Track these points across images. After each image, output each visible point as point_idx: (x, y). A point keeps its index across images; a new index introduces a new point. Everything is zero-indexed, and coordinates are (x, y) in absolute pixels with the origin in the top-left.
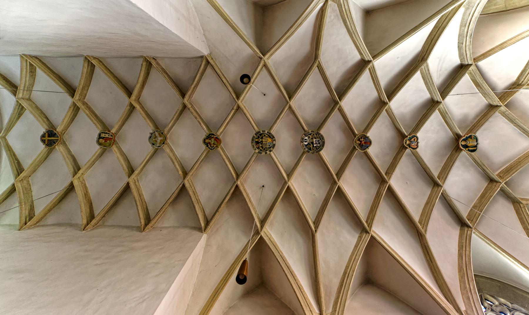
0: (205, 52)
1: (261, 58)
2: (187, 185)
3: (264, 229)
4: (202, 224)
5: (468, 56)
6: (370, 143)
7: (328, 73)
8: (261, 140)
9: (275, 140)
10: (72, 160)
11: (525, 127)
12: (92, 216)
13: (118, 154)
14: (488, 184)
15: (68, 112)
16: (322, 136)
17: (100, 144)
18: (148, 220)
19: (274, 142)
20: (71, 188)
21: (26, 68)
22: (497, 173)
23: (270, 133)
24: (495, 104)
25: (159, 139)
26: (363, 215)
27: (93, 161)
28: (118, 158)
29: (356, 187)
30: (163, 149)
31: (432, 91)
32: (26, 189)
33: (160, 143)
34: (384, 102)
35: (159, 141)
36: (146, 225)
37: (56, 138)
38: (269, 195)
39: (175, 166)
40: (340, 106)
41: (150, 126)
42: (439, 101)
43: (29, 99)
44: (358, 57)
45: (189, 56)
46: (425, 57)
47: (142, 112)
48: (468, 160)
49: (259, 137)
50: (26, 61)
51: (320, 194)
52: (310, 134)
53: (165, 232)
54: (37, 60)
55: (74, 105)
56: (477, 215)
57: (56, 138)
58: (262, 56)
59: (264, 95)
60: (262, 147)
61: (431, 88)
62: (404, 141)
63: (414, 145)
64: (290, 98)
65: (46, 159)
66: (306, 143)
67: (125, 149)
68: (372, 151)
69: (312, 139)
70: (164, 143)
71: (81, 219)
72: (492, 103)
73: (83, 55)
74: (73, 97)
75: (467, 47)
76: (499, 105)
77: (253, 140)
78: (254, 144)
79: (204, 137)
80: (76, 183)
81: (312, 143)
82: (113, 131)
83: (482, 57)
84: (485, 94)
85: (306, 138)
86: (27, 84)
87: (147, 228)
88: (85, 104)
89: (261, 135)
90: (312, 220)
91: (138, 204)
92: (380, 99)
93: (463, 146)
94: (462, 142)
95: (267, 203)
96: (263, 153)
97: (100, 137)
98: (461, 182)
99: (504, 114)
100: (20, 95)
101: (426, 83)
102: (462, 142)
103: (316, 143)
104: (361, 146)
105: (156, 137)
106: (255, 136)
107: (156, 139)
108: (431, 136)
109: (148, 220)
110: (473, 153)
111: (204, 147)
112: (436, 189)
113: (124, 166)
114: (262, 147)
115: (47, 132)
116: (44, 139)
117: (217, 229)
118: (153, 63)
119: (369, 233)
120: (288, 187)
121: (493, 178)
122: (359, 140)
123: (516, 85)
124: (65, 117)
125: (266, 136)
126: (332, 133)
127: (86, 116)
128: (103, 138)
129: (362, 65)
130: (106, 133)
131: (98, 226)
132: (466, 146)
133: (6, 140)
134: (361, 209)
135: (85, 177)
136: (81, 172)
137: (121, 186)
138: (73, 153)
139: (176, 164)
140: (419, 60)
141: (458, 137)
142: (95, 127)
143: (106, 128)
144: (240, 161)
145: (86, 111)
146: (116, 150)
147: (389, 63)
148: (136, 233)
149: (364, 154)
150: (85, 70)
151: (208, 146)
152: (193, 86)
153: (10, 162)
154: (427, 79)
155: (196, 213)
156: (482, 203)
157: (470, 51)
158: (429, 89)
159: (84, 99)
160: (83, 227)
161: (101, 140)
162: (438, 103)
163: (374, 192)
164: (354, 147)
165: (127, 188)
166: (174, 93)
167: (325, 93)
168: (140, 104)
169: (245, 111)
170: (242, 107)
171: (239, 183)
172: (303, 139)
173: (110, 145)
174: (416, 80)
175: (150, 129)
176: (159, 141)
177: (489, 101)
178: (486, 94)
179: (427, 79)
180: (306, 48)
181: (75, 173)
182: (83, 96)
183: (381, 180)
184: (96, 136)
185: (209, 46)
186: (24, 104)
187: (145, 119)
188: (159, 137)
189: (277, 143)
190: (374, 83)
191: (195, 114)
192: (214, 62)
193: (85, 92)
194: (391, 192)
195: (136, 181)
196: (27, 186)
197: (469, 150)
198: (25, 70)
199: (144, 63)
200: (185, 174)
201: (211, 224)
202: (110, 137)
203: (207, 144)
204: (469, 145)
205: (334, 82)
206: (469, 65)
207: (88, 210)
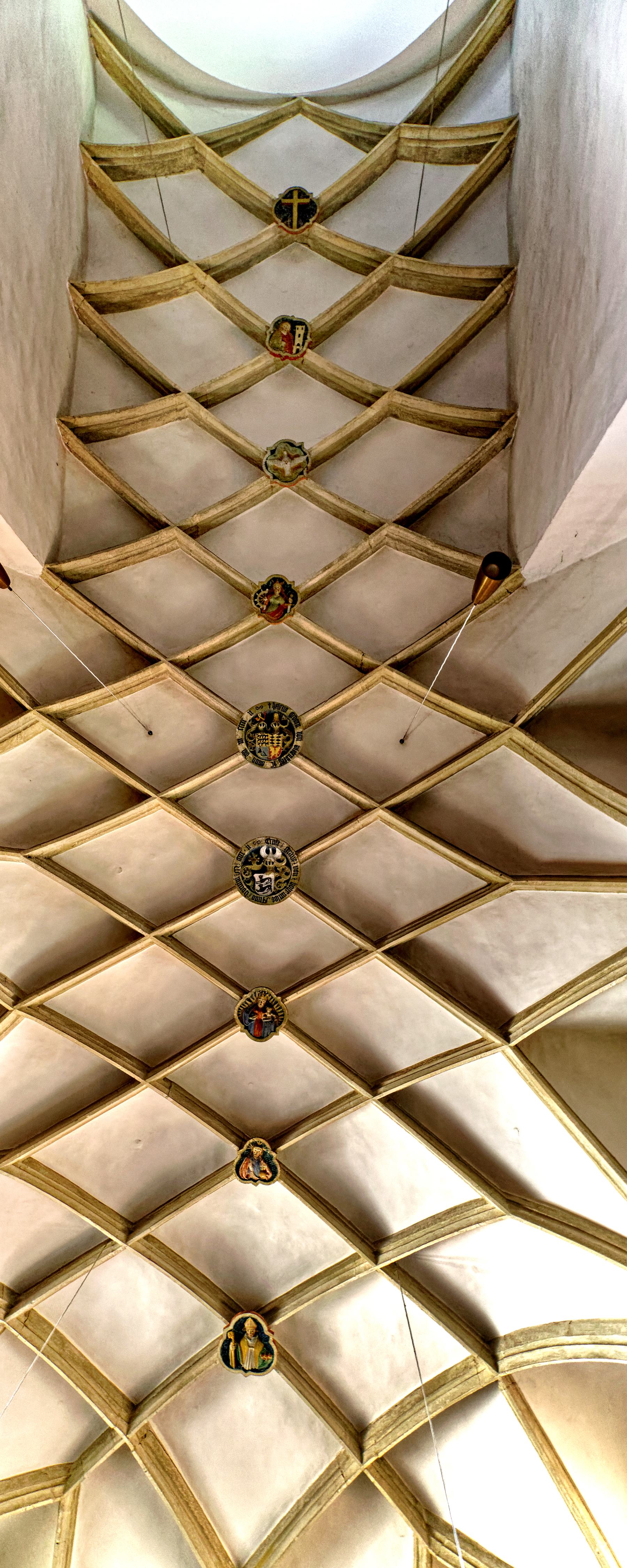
0: (533, 566)
1: (513, 721)
2: (164, 535)
3: (45, 721)
4: (70, 562)
5: (527, 1356)
6: (260, 1037)
7: (466, 917)
8: (276, 727)
9: (274, 766)
10: (239, 262)
11: (294, 1535)
12: (103, 306)
13: (249, 370)
14: (123, 1396)
15: (364, 246)
16: (283, 897)
17: (277, 324)
18: (88, 437)
19: (268, 764)
20: (169, 259)
21: (479, 138)
22: (155, 1429)
23: (294, 753)
24: (369, 1444)
25: (287, 467)
26: (65, 995)
27: (234, 312)
28: (241, 368)
29: (136, 985)
30: (260, 476)
31: (412, 1237)
32: (174, 161)
33: (276, 469)
34: (379, 1086)
35: (281, 465)
36: (74, 429)
37: (295, 223)
38: (131, 747)
39: (215, 506)
40: (366, 952)
41: (321, 443)
42: (382, 1258)
43: (395, 157)
44: (517, 1006)
45: (517, 529)
46: (522, 1211)
47: (358, 424)
48: (197, 1341)
49: (284, 723)
50: (499, 135)
51: (124, 885)
52: (288, 865)
53: (55, 473)
54: (501, 159)
55: (380, 258)
56: (37, 1341)
57: (295, 223)
58: (520, 722)
59: (402, 741)
60: (257, 730)
61: (421, 1232)
62: (264, 1143)
63: (250, 1168)
64: (396, 810)
65: (245, 206)
66: (263, 852)
67: (263, 388)
68: (237, 1040)
69: (275, 870)
70: (275, 477)
71: (100, 282)
72: (370, 1433)
73: (517, 264)
74: (402, 253)
75: (556, 1350)
76: (366, 1455)
77: (277, 705)
78: (266, 709)
79: (289, 579)
80: (182, 271)
81: (264, 870)
82: (311, 356)
83: (523, 1407)
84: (400, 1412)
85: (278, 854)
86: (438, 146)
87: (66, 429)
88: (383, 285)
89: (291, 729)
90: (57, 853)
91: (126, 414)
92: (388, 1077)
93: (240, 1325)
94: (253, 1323)
95: (106, 737)
96: (239, 734)
97: (294, 323)
98: (135, 1306)
99: (337, 1468)
100: (407, 134)
101: (435, 1219)
102: (253, 1323)
103: (262, 880)
104: (250, 1009)
105: (291, 458)
106: (289, 712)
107: (286, 459)
108: (271, 1225)
109: (88, 437)
110: (217, 1355)
111: (264, 579)
112: (120, 1226)
113: (220, 385)
114: (257, 730)
115: (312, 202)
116: (295, 194)
117: (47, 605)
118: (496, 439)
119: (14, 1004)
120: (149, 796)
121: (141, 1412)
122: (268, 1004)
123: (427, 1520)
124: (347, 240)
125: (288, 743)
126: (287, 929)
127: (350, 289)
128: (293, 331)
129: (496, 1018)
130: (305, 338)
131: (76, 321)
132: (239, 1332)
133: (294, 114)
134: (76, 994)
135: (197, 295)
136: (210, 282)
137: (171, 376)
138: (256, 266)
139: (221, 509)
140: (511, 1193)
141: (270, 1313)
142: (322, 311)
143: (319, 339)
144: (219, 673)
145: (363, 289)
146: (258, 366)
147: (499, 1096)
148: (56, 403)
149: (226, 1019)
150: (475, 275)
151: (264, 587)
152: (430, 545)
153: (240, 125)
154: (451, 1221)
155: (97, 552)
156: (70, 1362)
157: (544, 1359)
158: (417, 1227)
159: (397, 284)
160: (76, 283)
161: (287, 326)
162: (375, 1256)
163: (120, 1038)
164: (246, 992)
165: (161, 389)
166: (410, 498)
167: (407, 914)
168: (380, 419)
169: (358, 687)
170: (370, 679)
171: (164, 666)
172: (277, 842)
173: (275, 348)
174: (448, 1186)
175: (315, 443)
176: (281, 465)
177: (379, 1426)
178: (401, 1413)
179: (451, 1221)
180: (546, 850)
181: (207, 270)
182: (404, 281)
183: (152, 1062)
184: (298, 315)
185: (545, 581)
186: (383, 147)
187: (340, 430)
188: (294, 465)
189: (267, 771)
190: (437, 1057)
191: (352, 556)
192: (499, 599)
193: (414, 283)
194: (121, 1086)
195: (181, 414)
196: (179, 163)
197: (227, 1342)
198: (475, 135)
199: (494, 416)
200: (194, 532)
201: (65, 588)
202: (295, 348)
203: (269, 586)
204: (243, 1343)
205: (436, 935)
206: (494, 1362)
207: (117, 299)
